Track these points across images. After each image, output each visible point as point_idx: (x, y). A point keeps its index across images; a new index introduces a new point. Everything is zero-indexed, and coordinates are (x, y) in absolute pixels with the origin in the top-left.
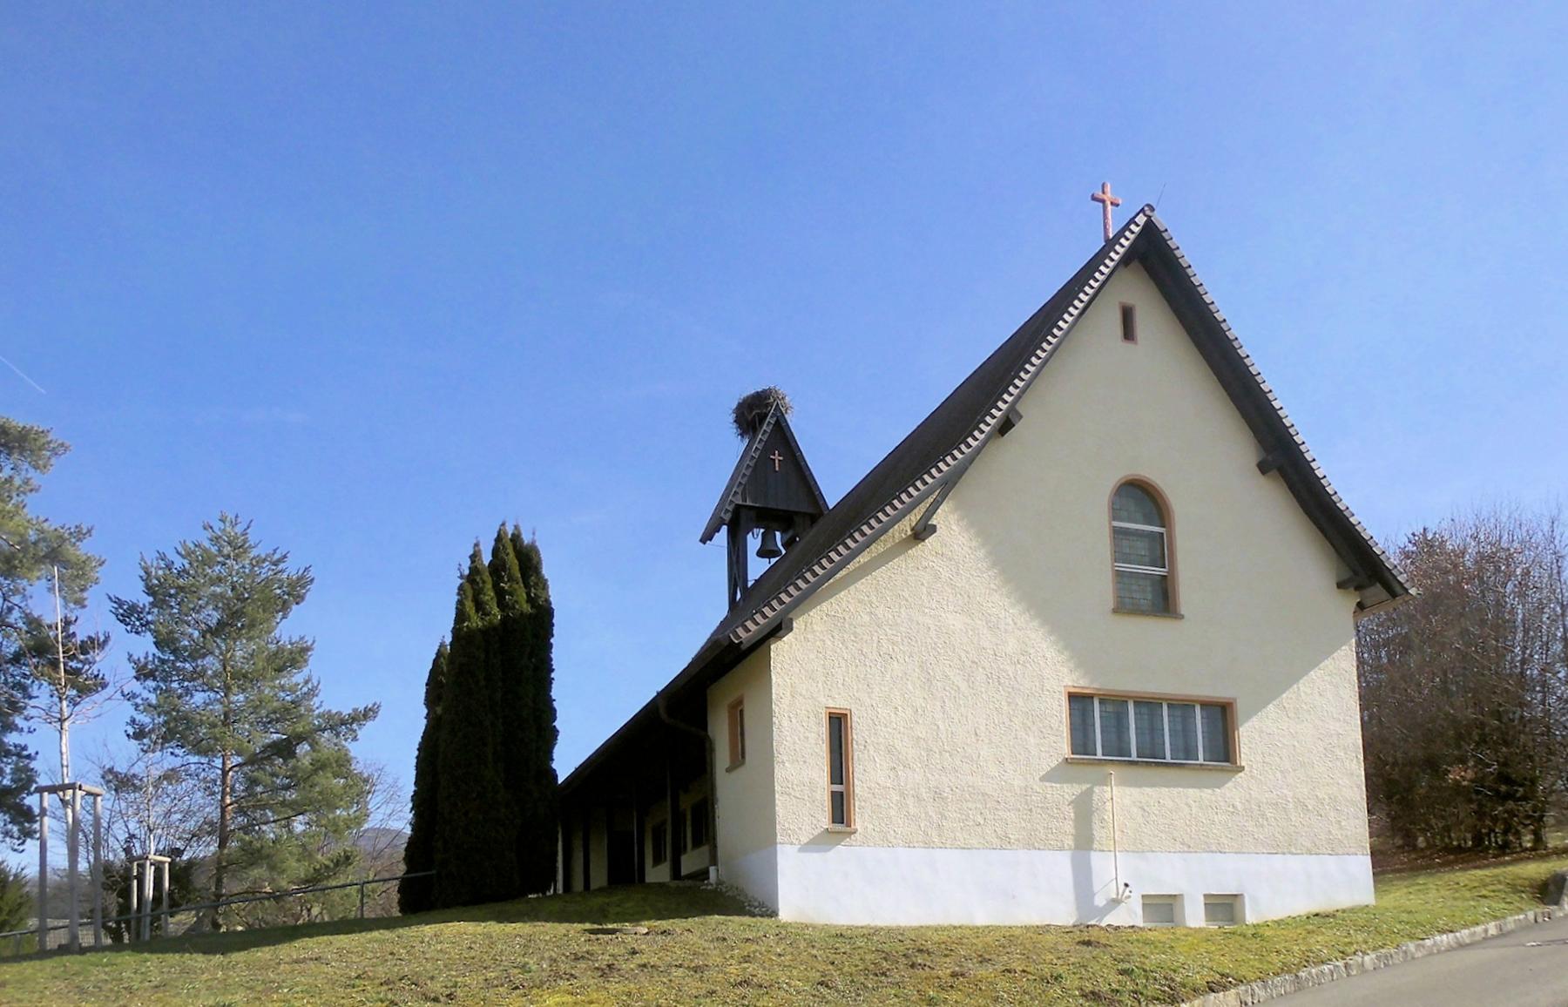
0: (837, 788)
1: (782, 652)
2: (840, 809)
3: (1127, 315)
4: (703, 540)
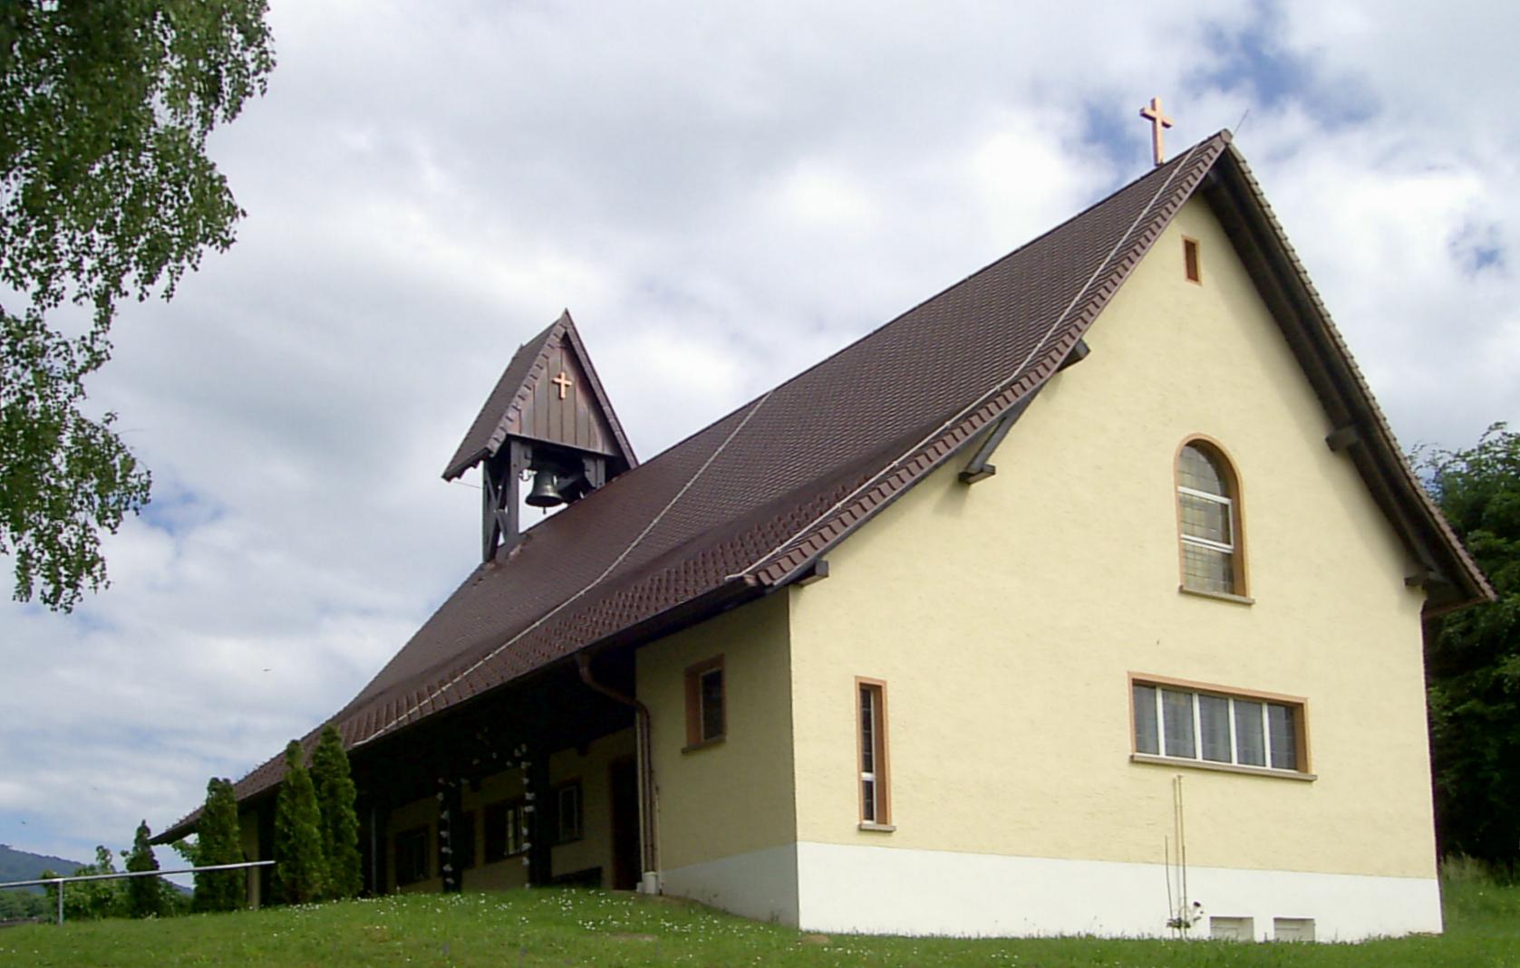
0: (867, 776)
1: (481, 561)
2: (874, 802)
3: (1190, 248)
4: (448, 476)
